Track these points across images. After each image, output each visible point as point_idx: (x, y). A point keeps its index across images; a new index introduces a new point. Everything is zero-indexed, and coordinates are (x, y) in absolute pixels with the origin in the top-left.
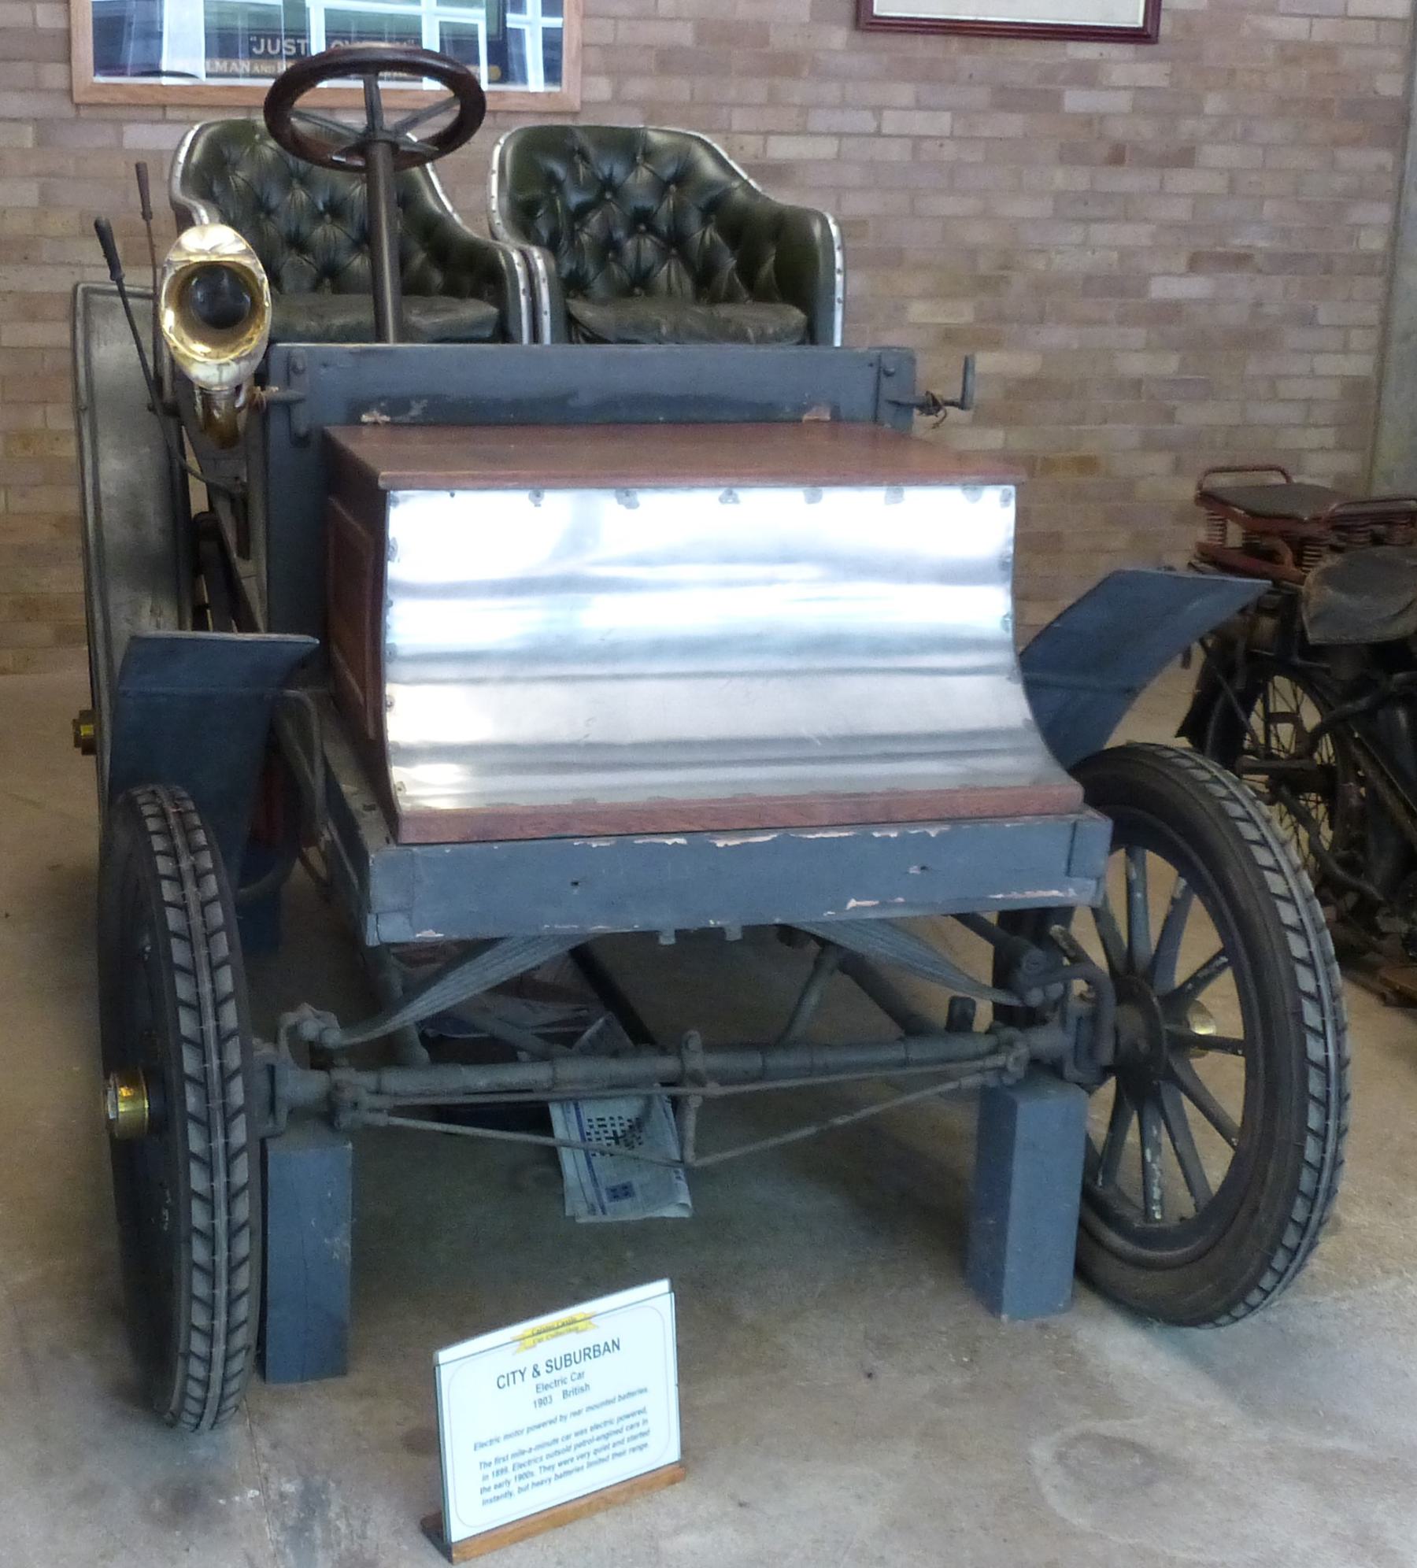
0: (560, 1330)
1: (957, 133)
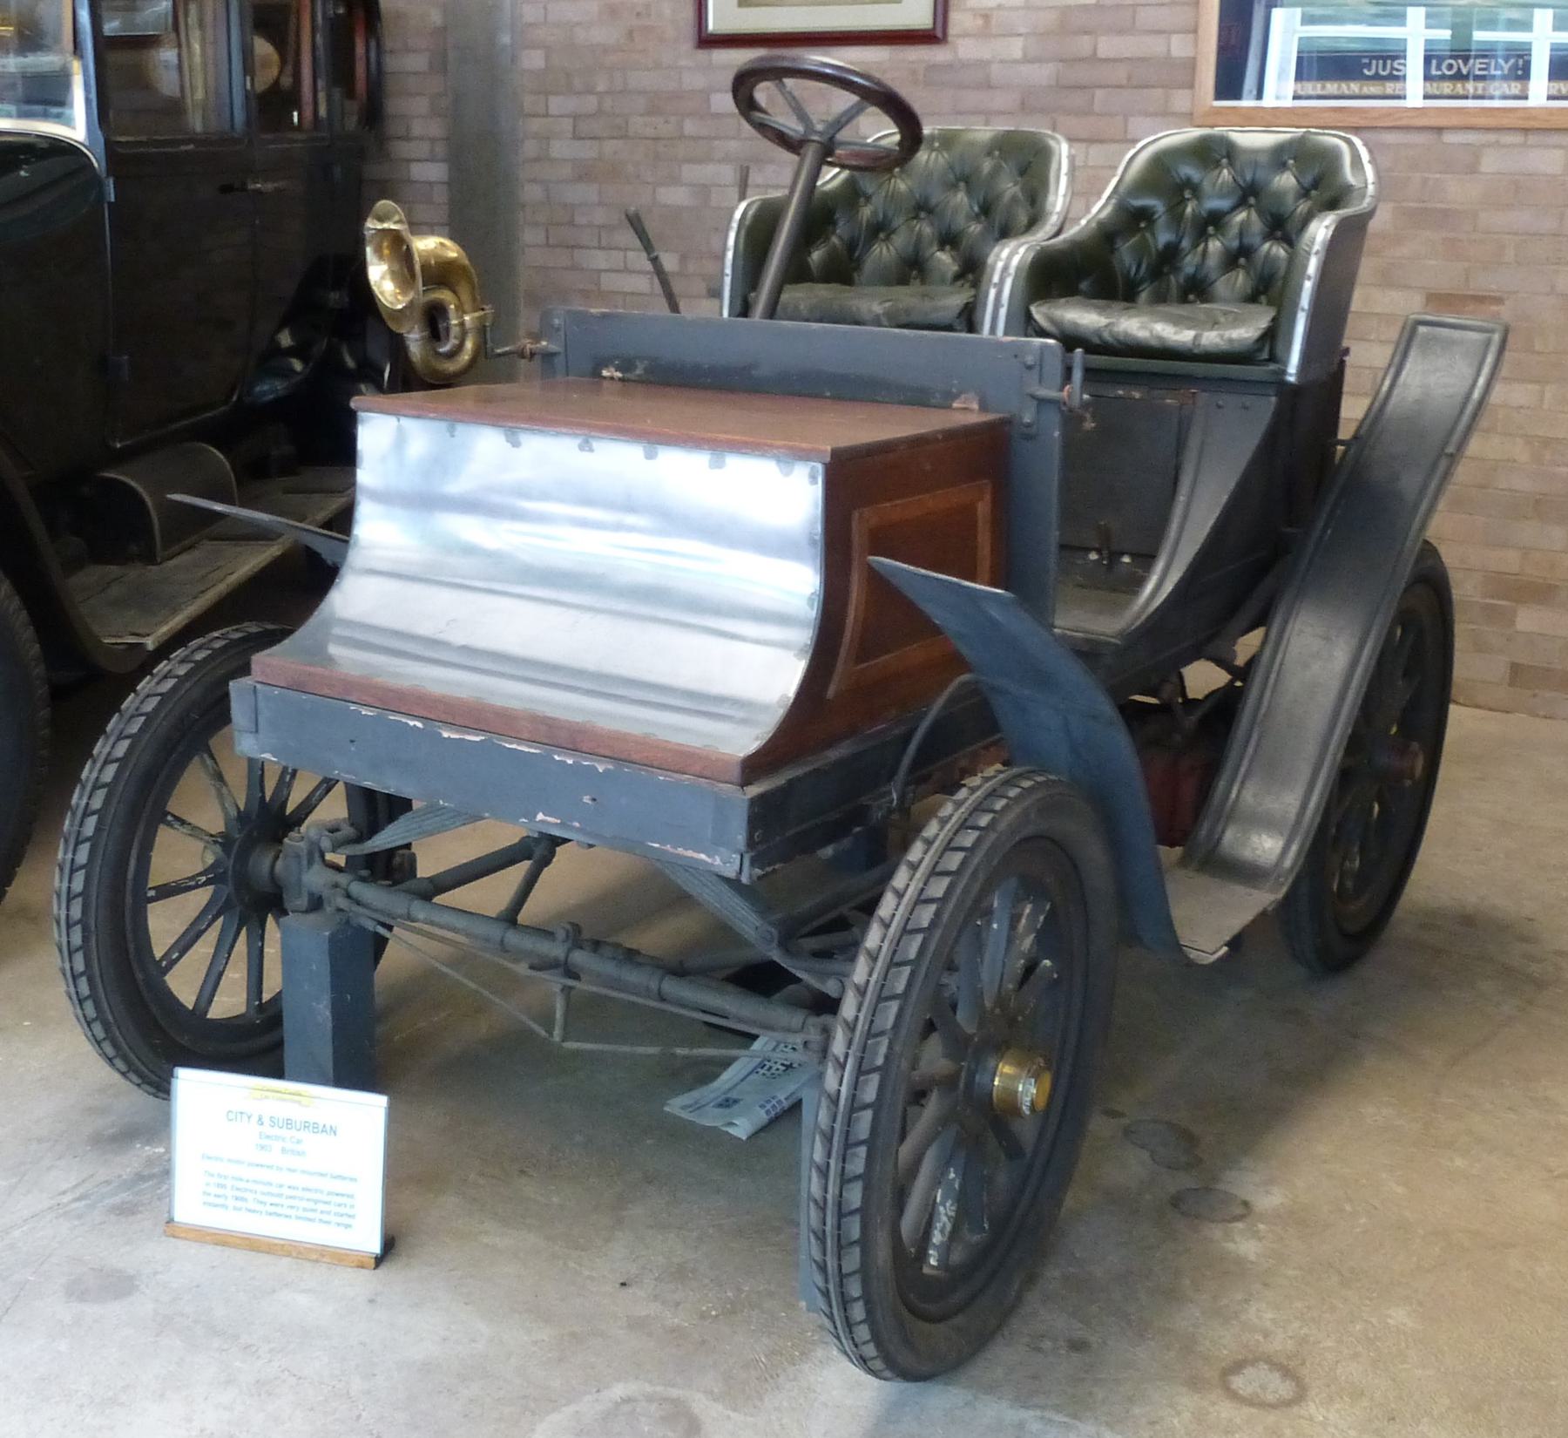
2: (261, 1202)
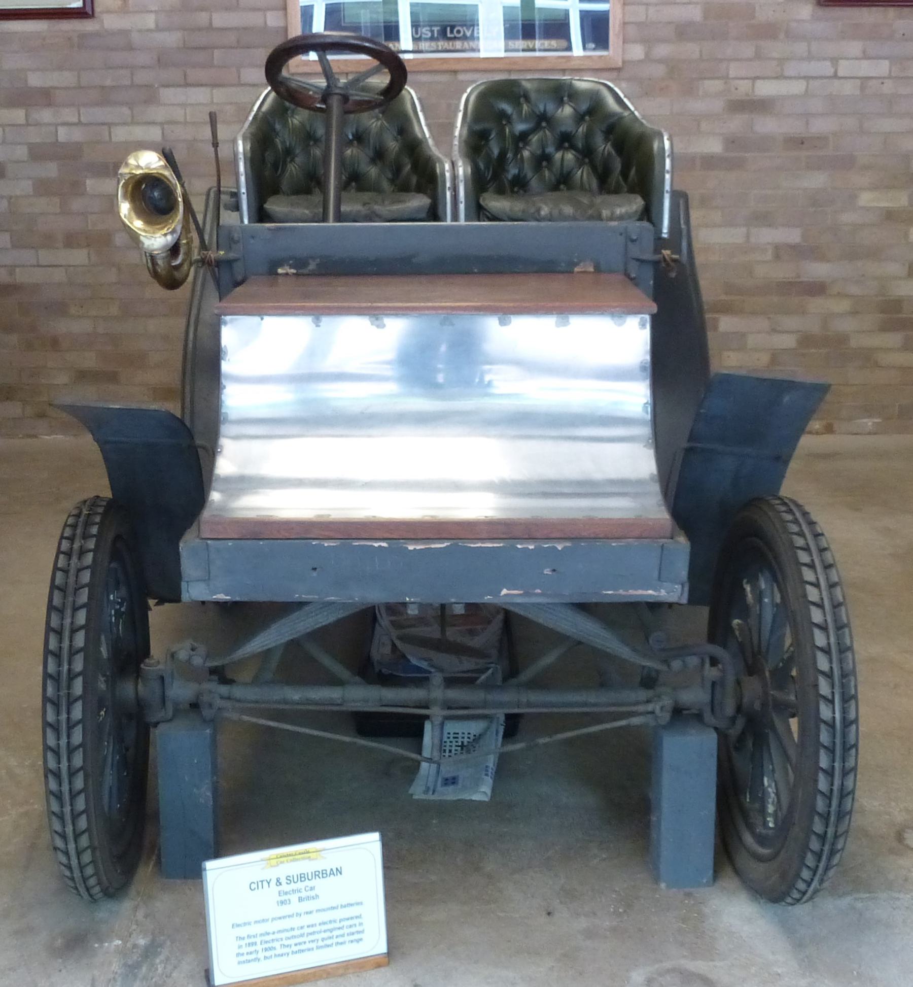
0: (296, 857)
1: (893, 74)
2: (288, 946)
